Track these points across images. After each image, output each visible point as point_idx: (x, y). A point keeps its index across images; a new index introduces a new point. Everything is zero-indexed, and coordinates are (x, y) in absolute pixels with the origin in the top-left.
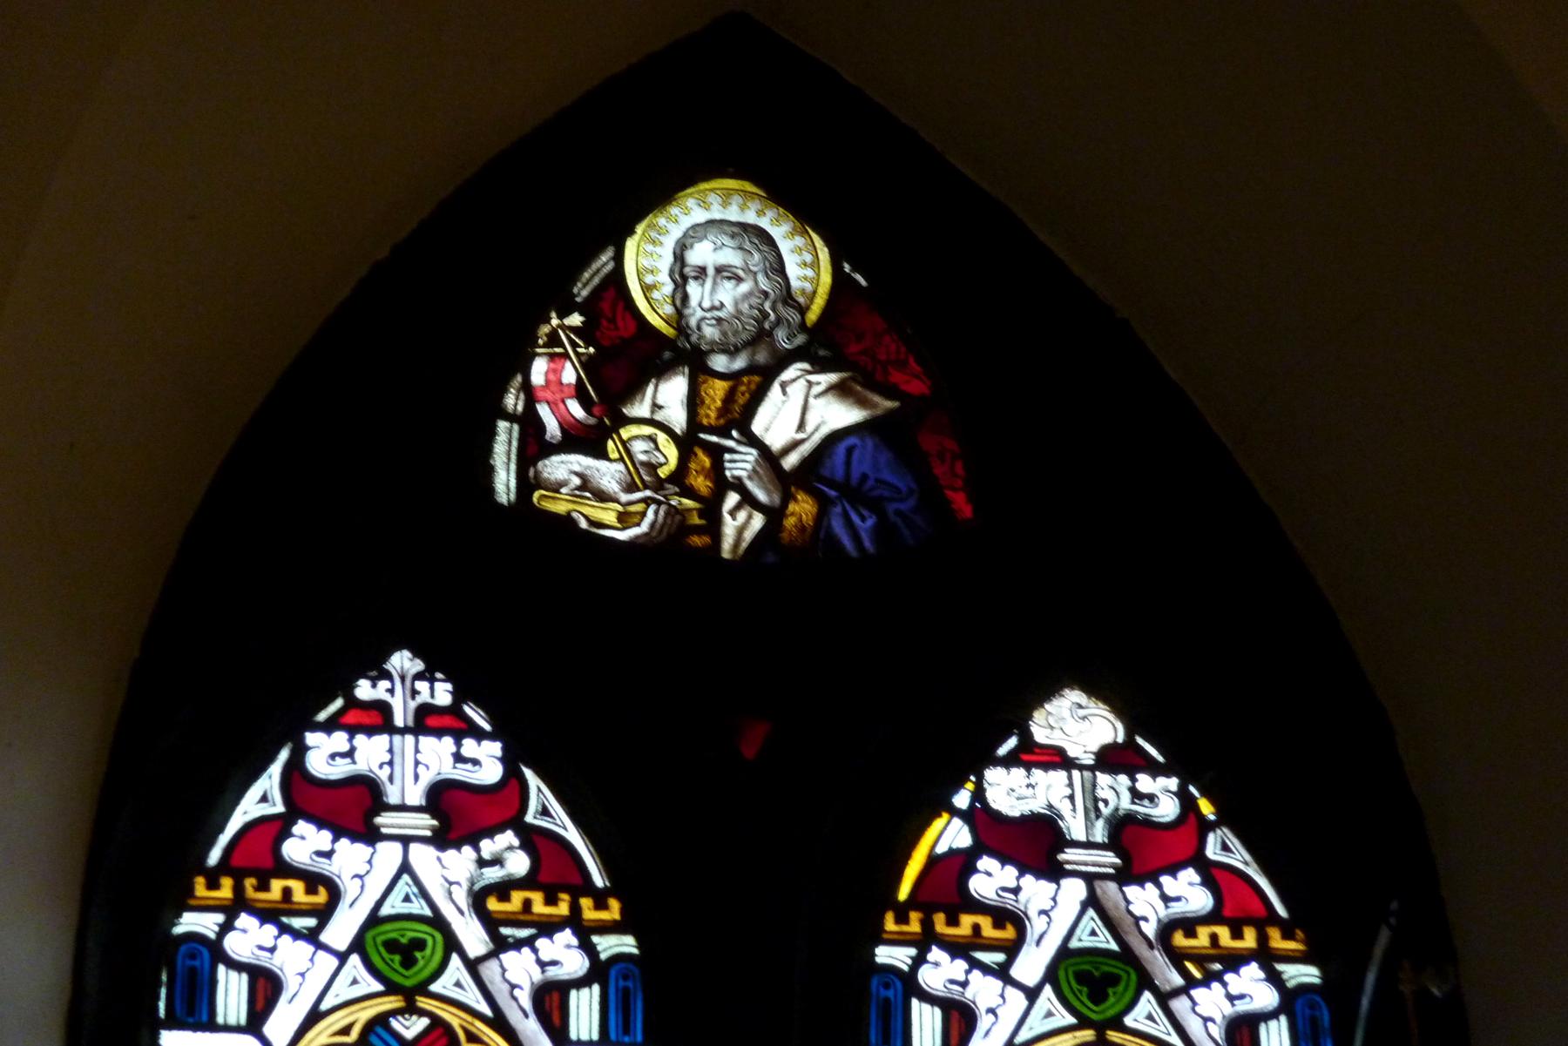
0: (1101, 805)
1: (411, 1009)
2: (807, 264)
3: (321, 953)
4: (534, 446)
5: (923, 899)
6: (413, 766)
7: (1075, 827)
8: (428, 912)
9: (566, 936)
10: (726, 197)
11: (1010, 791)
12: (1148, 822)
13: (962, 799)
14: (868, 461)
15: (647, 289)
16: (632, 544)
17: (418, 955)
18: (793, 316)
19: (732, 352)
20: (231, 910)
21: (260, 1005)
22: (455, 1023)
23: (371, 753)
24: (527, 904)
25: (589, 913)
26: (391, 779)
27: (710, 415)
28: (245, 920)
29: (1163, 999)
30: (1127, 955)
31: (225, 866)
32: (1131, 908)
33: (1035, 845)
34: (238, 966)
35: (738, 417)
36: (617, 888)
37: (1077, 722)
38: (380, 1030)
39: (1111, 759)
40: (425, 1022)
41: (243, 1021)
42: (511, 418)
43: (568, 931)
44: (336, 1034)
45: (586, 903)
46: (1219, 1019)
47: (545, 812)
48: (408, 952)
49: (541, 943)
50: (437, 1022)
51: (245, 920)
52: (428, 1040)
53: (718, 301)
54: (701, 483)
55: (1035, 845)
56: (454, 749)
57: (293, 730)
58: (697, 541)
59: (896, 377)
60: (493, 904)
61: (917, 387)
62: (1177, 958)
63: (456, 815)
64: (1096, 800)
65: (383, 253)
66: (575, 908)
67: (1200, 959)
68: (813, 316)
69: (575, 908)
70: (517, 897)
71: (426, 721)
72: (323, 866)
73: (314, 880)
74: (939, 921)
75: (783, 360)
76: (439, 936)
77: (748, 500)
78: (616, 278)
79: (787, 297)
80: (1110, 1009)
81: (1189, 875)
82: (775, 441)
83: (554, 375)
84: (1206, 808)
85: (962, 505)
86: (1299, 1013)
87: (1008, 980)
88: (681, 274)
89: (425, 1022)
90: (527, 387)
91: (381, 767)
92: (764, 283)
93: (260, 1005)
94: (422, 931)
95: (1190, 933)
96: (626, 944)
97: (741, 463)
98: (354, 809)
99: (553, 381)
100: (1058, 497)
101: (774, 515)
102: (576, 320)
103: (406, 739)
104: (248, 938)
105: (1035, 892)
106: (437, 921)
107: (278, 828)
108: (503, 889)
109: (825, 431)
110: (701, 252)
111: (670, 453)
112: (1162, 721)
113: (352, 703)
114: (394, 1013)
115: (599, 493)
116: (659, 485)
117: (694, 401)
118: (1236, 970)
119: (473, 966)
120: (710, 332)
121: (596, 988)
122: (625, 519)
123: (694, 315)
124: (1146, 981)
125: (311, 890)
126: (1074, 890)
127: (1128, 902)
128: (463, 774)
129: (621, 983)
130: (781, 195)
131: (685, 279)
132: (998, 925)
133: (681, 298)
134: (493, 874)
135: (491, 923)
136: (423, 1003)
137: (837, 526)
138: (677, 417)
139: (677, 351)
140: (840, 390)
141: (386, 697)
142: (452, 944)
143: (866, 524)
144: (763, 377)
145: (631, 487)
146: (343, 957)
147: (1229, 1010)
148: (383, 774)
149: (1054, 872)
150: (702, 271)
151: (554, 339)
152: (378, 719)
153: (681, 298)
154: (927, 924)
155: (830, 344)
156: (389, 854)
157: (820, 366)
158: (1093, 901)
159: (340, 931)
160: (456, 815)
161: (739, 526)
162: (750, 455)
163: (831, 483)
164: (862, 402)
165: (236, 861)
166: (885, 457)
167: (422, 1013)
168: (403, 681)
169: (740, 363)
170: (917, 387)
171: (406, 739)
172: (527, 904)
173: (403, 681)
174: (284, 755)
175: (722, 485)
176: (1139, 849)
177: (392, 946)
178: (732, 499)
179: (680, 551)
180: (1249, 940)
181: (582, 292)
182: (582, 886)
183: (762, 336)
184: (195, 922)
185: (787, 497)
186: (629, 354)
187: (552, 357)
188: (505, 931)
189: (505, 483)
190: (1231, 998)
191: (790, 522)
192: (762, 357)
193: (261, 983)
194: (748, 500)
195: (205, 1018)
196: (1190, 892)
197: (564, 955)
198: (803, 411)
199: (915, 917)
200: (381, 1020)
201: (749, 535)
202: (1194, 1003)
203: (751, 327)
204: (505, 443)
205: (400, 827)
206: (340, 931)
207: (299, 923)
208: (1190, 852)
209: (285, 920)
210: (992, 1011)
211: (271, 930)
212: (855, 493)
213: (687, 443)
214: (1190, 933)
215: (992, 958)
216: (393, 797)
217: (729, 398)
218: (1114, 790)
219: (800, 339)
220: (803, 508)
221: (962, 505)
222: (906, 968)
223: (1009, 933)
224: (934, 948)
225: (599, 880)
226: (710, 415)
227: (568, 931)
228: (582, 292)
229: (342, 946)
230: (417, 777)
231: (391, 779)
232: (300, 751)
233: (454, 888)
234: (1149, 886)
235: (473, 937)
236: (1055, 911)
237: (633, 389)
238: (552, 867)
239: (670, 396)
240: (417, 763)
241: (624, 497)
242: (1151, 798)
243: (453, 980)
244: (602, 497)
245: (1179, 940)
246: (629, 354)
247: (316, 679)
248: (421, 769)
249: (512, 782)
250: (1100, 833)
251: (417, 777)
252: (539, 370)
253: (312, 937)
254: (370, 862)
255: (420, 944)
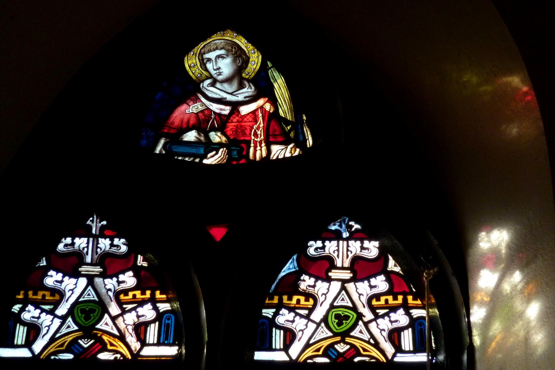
0: (349, 253)
1: (343, 341)
3: (310, 323)
8: (350, 305)
9: (401, 311)
17: (337, 321)
21: (31, 338)
22: (357, 345)
23: (331, 247)
24: (387, 301)
26: (338, 256)
28: (284, 311)
32: (358, 291)
34: (280, 327)
38: (331, 350)
40: (348, 347)
41: (412, 349)
43: (402, 309)
44: (57, 347)
45: (410, 298)
46: (386, 330)
49: (392, 315)
50: (353, 346)
51: (284, 311)
52: (350, 352)
56: (110, 242)
60: (374, 302)
64: (97, 247)
66: (405, 300)
71: (354, 236)
72: (311, 290)
73: (308, 296)
76: (331, 313)
81: (382, 278)
86: (416, 328)
87: (310, 320)
89: (348, 347)
91: (334, 252)
93: (288, 342)
95: (378, 300)
98: (71, 265)
104: (30, 313)
105: (69, 283)
106: (354, 308)
107: (295, 277)
108: (377, 297)
114: (337, 343)
118: (395, 312)
121: (410, 330)
125: (307, 300)
126: (336, 286)
127: (105, 285)
128: (365, 254)
129: (419, 327)
131: (205, 65)
132: (52, 295)
135: (373, 309)
136: (348, 340)
141: (338, 228)
142: (360, 316)
146: (318, 325)
147: (391, 327)
148: (335, 255)
154: (281, 300)
156: (83, 282)
158: (343, 288)
159: (318, 315)
167: (347, 343)
172: (134, 296)
184: (268, 313)
188: (124, 306)
190: (391, 322)
193: (288, 333)
195: (267, 346)
199: (400, 298)
200: (332, 346)
202: (378, 325)
205: (86, 271)
206: (318, 315)
207: (47, 307)
208: (131, 264)
209: (297, 311)
210: (302, 331)
211: (292, 314)
214: (378, 300)
215: (304, 312)
216: (339, 264)
222: (271, 317)
224: (29, 305)
227: (402, 309)
229: (318, 321)
230: (348, 256)
231: (338, 256)
233: (361, 296)
234: (366, 282)
240: (348, 250)
242: (117, 246)
243: (359, 331)
248: (349, 253)
251: (348, 256)
253: (307, 317)
254: (76, 284)
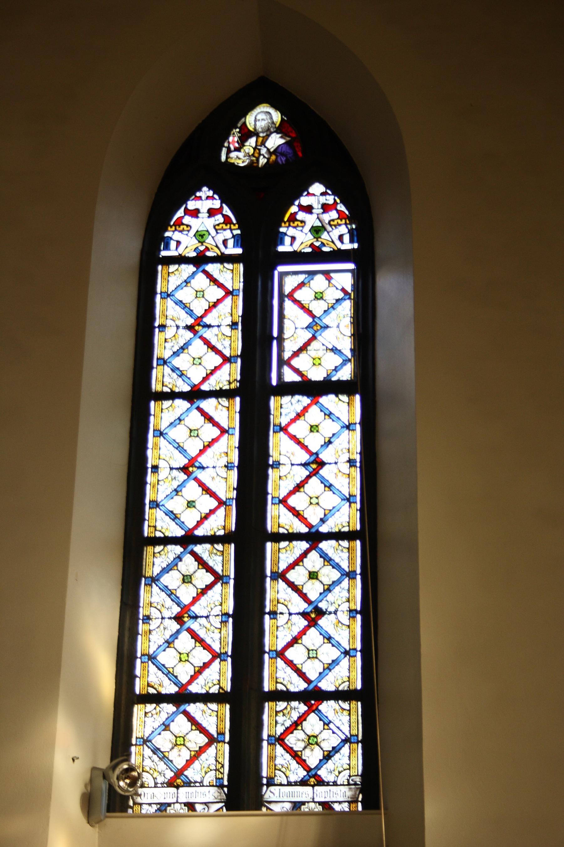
2: (277, 117)
4: (229, 151)
5: (289, 220)
6: (204, 206)
7: (315, 206)
10: (260, 108)
11: (305, 201)
12: (328, 204)
13: (297, 203)
14: (285, 149)
15: (250, 124)
16: (245, 166)
18: (273, 126)
19: (263, 132)
20: (288, 227)
25: (233, 227)
27: (259, 143)
29: (328, 233)
30: (323, 226)
31: (174, 225)
33: (308, 209)
35: (263, 144)
36: (237, 223)
37: (317, 188)
39: (323, 194)
42: (226, 147)
47: (226, 211)
48: (202, 236)
53: (261, 125)
54: (256, 155)
55: (308, 209)
57: (185, 201)
58: (255, 165)
59: (291, 134)
60: (217, 227)
61: (294, 135)
62: (331, 226)
63: (212, 213)
65: (200, 122)
66: (230, 227)
67: (335, 226)
68: (277, 125)
69: (230, 227)
70: (221, 226)
74: (177, 227)
75: (272, 133)
77: (264, 157)
78: (245, 123)
79: (273, 123)
80: (319, 235)
82: (269, 147)
83: (233, 139)
84: (338, 201)
85: (300, 154)
88: (256, 120)
90: (229, 143)
92: (269, 121)
94: (205, 233)
96: (239, 232)
97: (264, 151)
98: (195, 213)
99: (233, 141)
100: (319, 152)
101: (268, 159)
102: (238, 130)
103: (205, 200)
109: (278, 144)
110: (262, 116)
111: (252, 151)
112: (332, 186)
113: (196, 196)
115: (240, 159)
116: (249, 156)
117: (257, 142)
119: (213, 237)
120: (260, 130)
122: (243, 162)
123: (258, 127)
124: (325, 230)
128: (327, 202)
130: (273, 106)
133: (255, 125)
134: (217, 222)
135: (216, 230)
136: (319, 239)
137: (279, 160)
138: (254, 145)
139: (255, 134)
140: (281, 137)
143: (284, 159)
144: (268, 136)
145: (245, 156)
149: (311, 213)
150: (259, 120)
151: (234, 134)
152: (200, 198)
153: (255, 125)
155: (280, 129)
157: (278, 133)
158: (318, 218)
160: (212, 213)
161: (262, 161)
162: (265, 150)
163: (279, 153)
164: (284, 139)
165: (176, 224)
166: (288, 148)
168: (205, 192)
169: (265, 134)
170: (294, 135)
171: (205, 200)
173: (205, 192)
174: (184, 206)
175: (260, 154)
176: (326, 208)
177: (200, 235)
178: (262, 157)
179: (252, 167)
180: (344, 221)
181: (239, 125)
182: (231, 222)
183: (268, 129)
185: (271, 156)
186: (246, 134)
187: (234, 137)
189: (223, 158)
191: (271, 160)
192: (268, 133)
194: (264, 157)
196: (333, 215)
197: (228, 234)
198: (275, 141)
201: (264, 163)
203: (267, 128)
204: (224, 151)
212: (282, 154)
213: (255, 149)
217: (262, 141)
218: (323, 200)
219: (275, 130)
220: (273, 157)
221: (300, 154)
223: (303, 224)
225: (234, 221)
226: (259, 143)
228: (239, 125)
232: (187, 205)
235: (213, 232)
236: (311, 220)
237: (246, 140)
238: (227, 221)
239: (252, 141)
241: (243, 159)
244: (239, 159)
245: (332, 223)
246: (246, 134)
247: (190, 192)
249: (222, 207)
250: (320, 206)
252: (231, 139)
255: (204, 235)
